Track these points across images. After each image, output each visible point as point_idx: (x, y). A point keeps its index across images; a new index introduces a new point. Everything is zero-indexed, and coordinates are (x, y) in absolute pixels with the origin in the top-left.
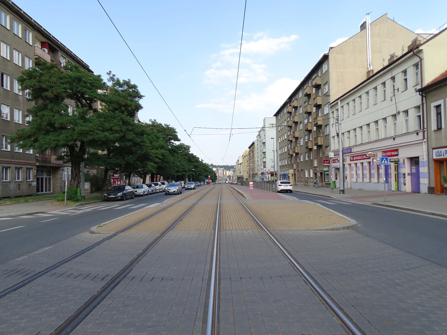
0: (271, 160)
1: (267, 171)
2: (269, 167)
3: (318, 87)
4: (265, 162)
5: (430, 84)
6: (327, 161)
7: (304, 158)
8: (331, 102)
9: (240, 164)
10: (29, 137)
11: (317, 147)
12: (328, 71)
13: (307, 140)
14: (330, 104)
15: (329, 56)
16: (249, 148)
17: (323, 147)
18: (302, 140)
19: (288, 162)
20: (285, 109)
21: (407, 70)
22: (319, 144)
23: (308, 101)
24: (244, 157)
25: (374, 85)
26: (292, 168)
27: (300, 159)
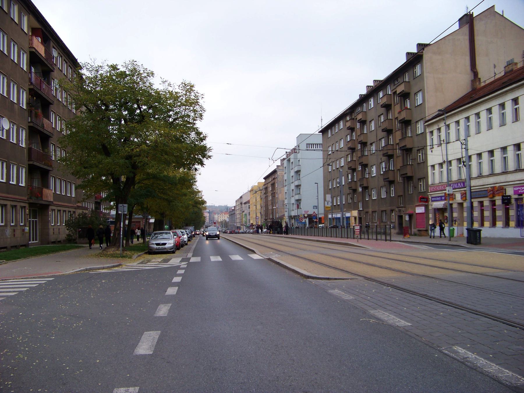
0: (312, 196)
1: (303, 213)
2: (308, 207)
3: (405, 96)
4: (470, 165)
5: (32, 255)
6: (423, 198)
7: (379, 194)
8: (427, 118)
9: (245, 203)
10: (439, 350)
11: (362, 189)
12: (422, 75)
13: (350, 180)
14: (426, 122)
15: (424, 56)
16: (265, 178)
17: (415, 180)
18: (374, 169)
19: (346, 200)
20: (341, 123)
21: (506, 103)
22: (364, 185)
23: (385, 113)
24: (253, 191)
25: (466, 115)
26: (356, 208)
27: (370, 196)
